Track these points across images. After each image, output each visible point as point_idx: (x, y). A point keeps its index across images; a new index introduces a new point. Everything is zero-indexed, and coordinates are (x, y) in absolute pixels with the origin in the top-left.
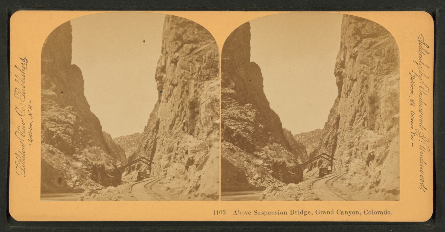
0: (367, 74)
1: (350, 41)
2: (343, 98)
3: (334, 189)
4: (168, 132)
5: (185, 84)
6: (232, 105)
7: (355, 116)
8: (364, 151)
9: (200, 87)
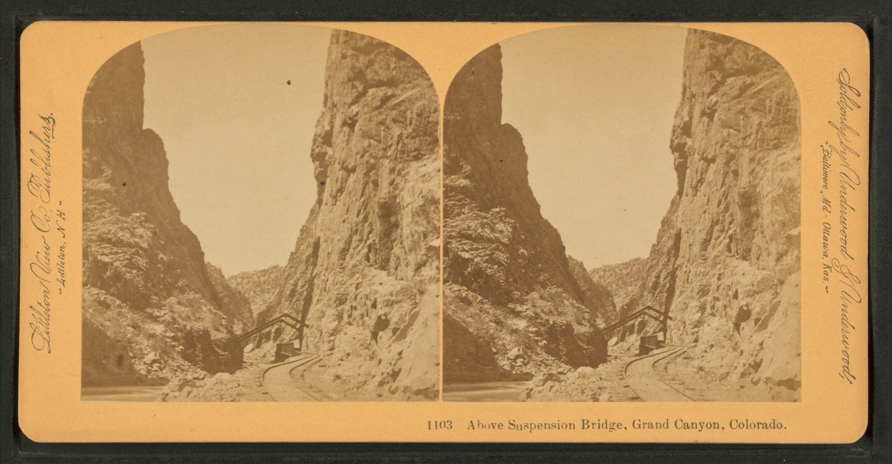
0: (736, 147)
1: (701, 82)
2: (687, 195)
3: (670, 377)
4: (336, 263)
5: (371, 168)
6: (466, 210)
7: (712, 232)
8: (730, 301)
9: (401, 174)
